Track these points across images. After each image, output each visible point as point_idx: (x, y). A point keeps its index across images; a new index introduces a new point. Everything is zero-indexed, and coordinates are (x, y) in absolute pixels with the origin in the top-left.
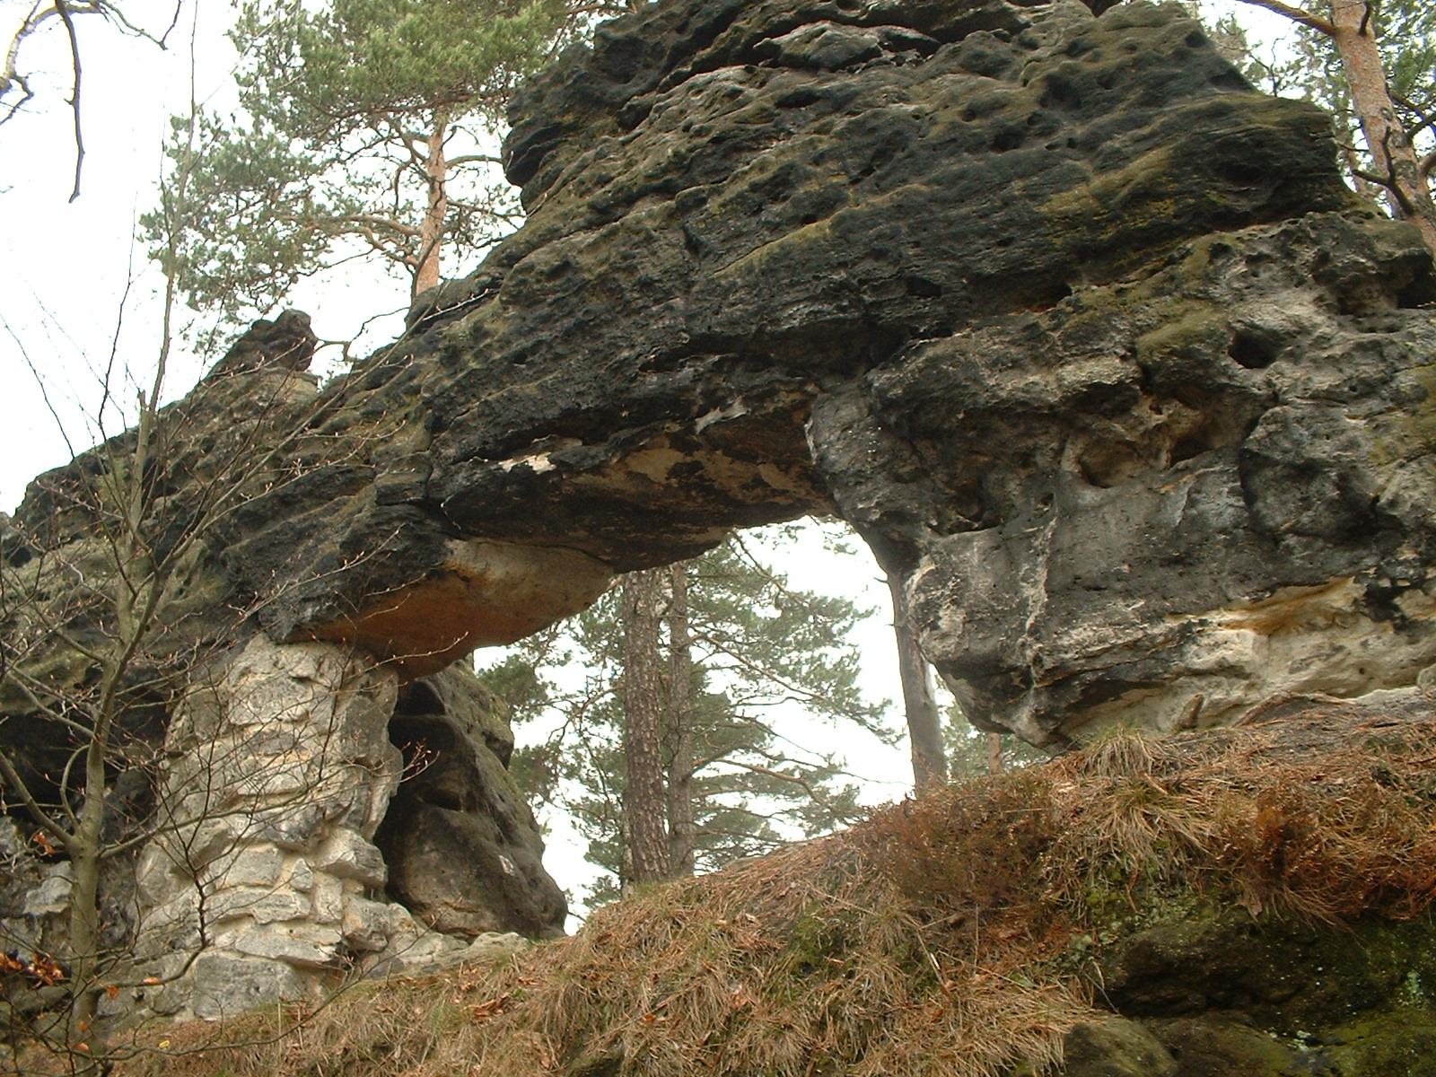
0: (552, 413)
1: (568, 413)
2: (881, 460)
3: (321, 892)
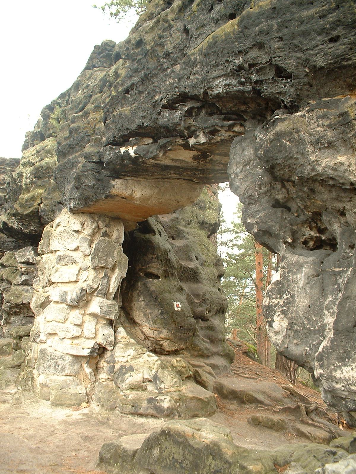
0: (134, 127)
1: (140, 127)
2: (264, 189)
3: (86, 325)
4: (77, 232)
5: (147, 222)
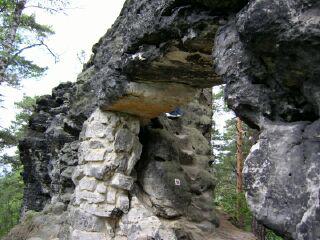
3: (109, 193)
4: (105, 124)
5: (157, 118)
